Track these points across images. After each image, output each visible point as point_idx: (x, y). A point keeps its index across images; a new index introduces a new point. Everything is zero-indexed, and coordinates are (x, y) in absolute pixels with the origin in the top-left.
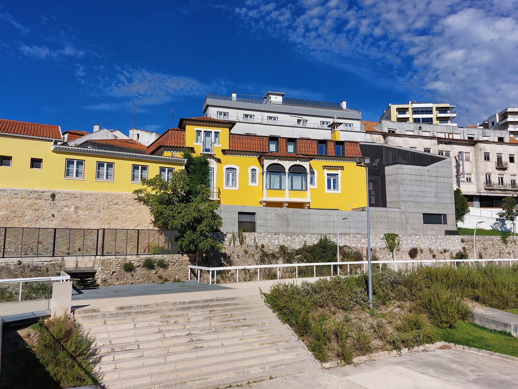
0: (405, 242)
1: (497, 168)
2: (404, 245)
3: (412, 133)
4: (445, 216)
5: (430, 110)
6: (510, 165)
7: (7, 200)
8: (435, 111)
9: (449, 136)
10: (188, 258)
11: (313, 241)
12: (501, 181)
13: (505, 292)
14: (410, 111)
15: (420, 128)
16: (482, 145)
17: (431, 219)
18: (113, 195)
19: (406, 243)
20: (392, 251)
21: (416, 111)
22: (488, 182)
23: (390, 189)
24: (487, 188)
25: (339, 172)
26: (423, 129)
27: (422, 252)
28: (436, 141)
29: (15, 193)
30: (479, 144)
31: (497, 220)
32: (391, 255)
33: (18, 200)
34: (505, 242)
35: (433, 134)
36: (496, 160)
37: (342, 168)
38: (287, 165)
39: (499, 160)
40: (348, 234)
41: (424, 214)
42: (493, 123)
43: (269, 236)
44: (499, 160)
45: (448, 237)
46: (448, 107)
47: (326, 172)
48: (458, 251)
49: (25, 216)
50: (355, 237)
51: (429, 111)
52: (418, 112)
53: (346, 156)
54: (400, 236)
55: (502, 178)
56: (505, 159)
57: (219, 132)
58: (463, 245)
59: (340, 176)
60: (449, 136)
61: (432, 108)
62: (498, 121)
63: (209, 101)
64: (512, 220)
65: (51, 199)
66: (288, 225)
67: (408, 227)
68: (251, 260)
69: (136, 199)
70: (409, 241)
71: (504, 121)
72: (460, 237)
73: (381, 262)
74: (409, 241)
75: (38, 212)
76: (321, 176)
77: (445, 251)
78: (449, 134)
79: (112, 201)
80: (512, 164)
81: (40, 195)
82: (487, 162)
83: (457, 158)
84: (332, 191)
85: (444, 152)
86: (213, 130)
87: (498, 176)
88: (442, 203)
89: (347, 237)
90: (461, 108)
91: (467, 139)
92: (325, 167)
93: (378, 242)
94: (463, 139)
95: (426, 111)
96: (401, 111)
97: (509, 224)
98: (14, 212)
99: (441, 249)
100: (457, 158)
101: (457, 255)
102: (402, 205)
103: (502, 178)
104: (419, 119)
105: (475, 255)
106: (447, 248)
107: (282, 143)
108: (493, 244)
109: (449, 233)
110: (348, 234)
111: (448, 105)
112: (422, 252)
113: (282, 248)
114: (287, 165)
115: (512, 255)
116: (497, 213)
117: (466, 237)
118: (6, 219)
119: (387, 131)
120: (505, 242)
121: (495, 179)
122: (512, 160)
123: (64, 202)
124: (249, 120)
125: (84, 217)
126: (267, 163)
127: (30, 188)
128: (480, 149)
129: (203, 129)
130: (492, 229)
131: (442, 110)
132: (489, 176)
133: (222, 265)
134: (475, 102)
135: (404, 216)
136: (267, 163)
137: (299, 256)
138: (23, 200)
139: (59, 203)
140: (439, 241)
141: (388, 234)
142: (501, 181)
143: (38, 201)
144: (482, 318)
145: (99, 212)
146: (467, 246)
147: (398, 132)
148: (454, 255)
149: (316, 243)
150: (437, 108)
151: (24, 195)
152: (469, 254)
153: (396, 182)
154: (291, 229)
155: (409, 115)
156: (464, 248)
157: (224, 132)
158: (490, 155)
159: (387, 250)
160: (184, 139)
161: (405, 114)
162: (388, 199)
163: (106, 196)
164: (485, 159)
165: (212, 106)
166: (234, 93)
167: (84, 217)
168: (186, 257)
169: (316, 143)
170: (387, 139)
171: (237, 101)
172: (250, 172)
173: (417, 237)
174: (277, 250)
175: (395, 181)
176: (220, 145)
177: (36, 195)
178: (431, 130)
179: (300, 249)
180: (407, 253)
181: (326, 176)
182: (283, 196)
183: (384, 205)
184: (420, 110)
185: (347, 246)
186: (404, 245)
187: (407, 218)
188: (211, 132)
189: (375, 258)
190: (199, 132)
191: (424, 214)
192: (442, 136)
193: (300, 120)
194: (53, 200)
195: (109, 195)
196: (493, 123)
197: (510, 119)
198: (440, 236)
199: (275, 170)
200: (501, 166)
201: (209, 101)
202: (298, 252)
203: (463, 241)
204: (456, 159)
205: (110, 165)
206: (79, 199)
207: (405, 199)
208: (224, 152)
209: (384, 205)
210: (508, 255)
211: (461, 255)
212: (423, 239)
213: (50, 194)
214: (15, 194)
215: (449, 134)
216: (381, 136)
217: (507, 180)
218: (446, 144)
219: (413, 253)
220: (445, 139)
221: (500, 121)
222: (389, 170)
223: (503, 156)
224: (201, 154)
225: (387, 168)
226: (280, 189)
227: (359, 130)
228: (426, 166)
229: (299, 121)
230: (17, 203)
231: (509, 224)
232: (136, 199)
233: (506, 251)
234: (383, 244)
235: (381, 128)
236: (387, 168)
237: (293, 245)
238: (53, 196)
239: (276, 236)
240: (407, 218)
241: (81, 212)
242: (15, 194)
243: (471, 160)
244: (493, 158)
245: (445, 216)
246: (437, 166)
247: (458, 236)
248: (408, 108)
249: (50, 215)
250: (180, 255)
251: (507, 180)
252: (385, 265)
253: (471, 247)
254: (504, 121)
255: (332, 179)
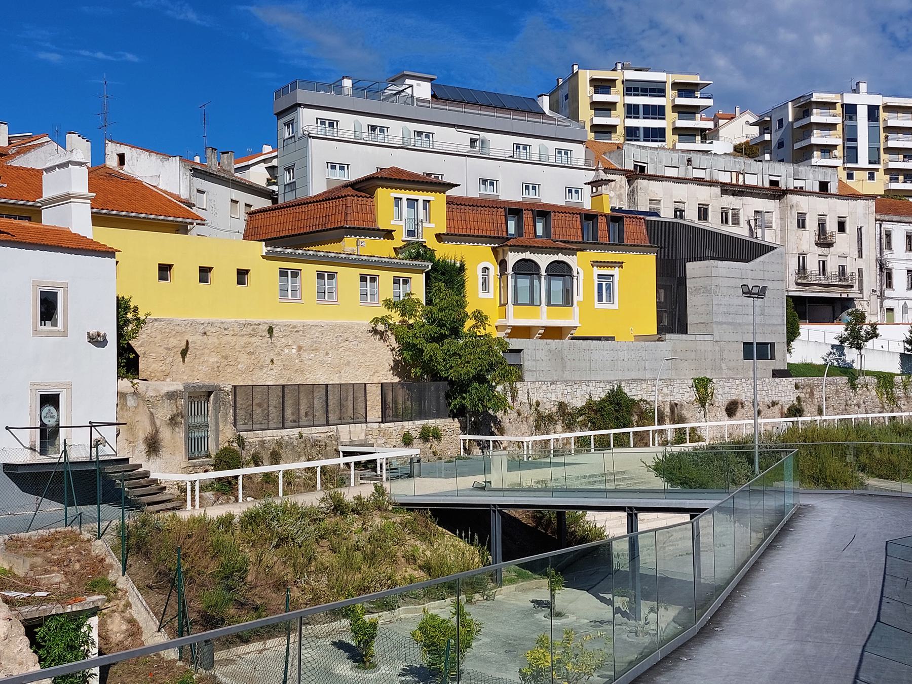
0: (721, 391)
1: (817, 244)
2: (719, 397)
3: (672, 173)
4: (773, 345)
5: (660, 86)
6: (839, 238)
7: (216, 340)
8: (670, 92)
9: (737, 179)
10: (459, 425)
11: (599, 393)
12: (823, 266)
13: (894, 458)
14: (619, 86)
15: (689, 161)
16: (793, 199)
17: (758, 351)
18: (342, 326)
19: (722, 394)
20: (703, 406)
21: (631, 88)
22: (802, 269)
23: (694, 301)
24: (799, 281)
25: (615, 271)
26: (695, 163)
27: (742, 407)
28: (717, 190)
29: (225, 328)
30: (789, 196)
31: (833, 346)
32: (702, 412)
33: (229, 338)
34: (854, 387)
35: (711, 173)
36: (817, 228)
37: (620, 264)
38: (543, 260)
39: (822, 226)
40: (645, 380)
41: (744, 343)
42: (781, 122)
43: (544, 387)
44: (822, 226)
45: (777, 380)
46: (698, 84)
47: (597, 271)
48: (791, 403)
49: (239, 363)
50: (654, 385)
51: (658, 90)
52: (636, 89)
53: (625, 242)
54: (714, 381)
55: (824, 262)
56: (831, 226)
57: (429, 201)
58: (798, 393)
59: (616, 278)
60: (737, 179)
61: (665, 82)
62: (790, 120)
63: (302, 95)
64: (859, 348)
65: (268, 336)
66: (564, 368)
67: (723, 366)
68: (524, 427)
69: (370, 331)
70: (727, 389)
71: (804, 122)
72: (792, 380)
73: (687, 426)
74: (727, 389)
75: (253, 357)
76: (588, 277)
77: (774, 404)
78: (738, 173)
79: (343, 333)
80: (842, 235)
81: (250, 329)
82: (801, 231)
83: (752, 223)
84: (605, 305)
85: (730, 212)
86: (421, 196)
87: (818, 258)
88: (769, 325)
89: (644, 386)
90: (665, 32)
91: (767, 185)
92: (596, 264)
93: (685, 394)
94: (760, 185)
95: (653, 90)
96: (602, 86)
97: (851, 355)
98: (226, 358)
99: (768, 400)
100: (752, 223)
101: (789, 409)
102: (717, 330)
103: (824, 262)
104: (636, 107)
105: (814, 409)
106: (776, 399)
107: (527, 217)
108: (837, 391)
109: (777, 374)
110: (645, 380)
111: (696, 79)
112: (742, 407)
113: (562, 406)
114: (543, 260)
115: (862, 409)
116: (836, 335)
117: (801, 380)
118: (216, 369)
119: (632, 168)
120: (854, 387)
121: (812, 266)
122: (842, 227)
123: (283, 340)
124: (380, 138)
125: (310, 363)
126: (513, 258)
127: (242, 320)
128: (792, 207)
129: (405, 195)
130: (824, 362)
131: (685, 89)
132: (804, 258)
133: (492, 434)
134: (699, 18)
135: (717, 348)
136: (513, 258)
137: (581, 418)
138: (234, 338)
139: (280, 340)
140: (765, 388)
141: (698, 379)
142: (823, 266)
143: (253, 339)
144: (877, 488)
145: (327, 354)
146: (802, 395)
147: (650, 171)
148: (785, 410)
149: (603, 396)
150: (675, 85)
151: (237, 330)
152: (805, 408)
153: (707, 290)
154: (567, 375)
155: (615, 96)
156: (798, 398)
157: (438, 200)
158: (807, 216)
159: (697, 405)
160: (373, 213)
161: (609, 93)
162: (690, 319)
163: (333, 327)
164: (799, 227)
165: (307, 106)
166: (348, 78)
167: (310, 363)
168: (456, 424)
169: (579, 219)
170: (635, 184)
171: (353, 95)
172: (480, 273)
173: (737, 382)
174: (554, 410)
175: (706, 287)
176: (432, 225)
177: (249, 330)
178: (708, 166)
179: (583, 407)
180: (724, 408)
181: (596, 277)
182: (537, 316)
183: (685, 331)
184: (640, 86)
185: (645, 401)
186: (719, 397)
187: (721, 351)
188: (417, 200)
189: (682, 420)
190: (398, 200)
191: (744, 343)
192: (725, 178)
193: (476, 140)
194: (271, 337)
195: (337, 326)
196: (781, 122)
197: (817, 117)
198: (767, 380)
199: (526, 269)
200: (824, 241)
201: (302, 95)
202: (581, 412)
203: (797, 387)
204: (750, 226)
205: (332, 276)
206: (301, 333)
207: (720, 319)
208: (439, 237)
209: (685, 331)
210: (856, 408)
211: (795, 411)
212: (744, 385)
213: (266, 327)
214: (225, 329)
215: (738, 173)
216: (624, 178)
217: (832, 268)
218: (733, 195)
219: (732, 409)
220: (731, 185)
221: (796, 119)
222: (692, 268)
223: (827, 219)
224: (403, 241)
225: (690, 266)
226: (532, 303)
227: (581, 163)
228: (747, 261)
229: (473, 141)
230: (228, 343)
231: (851, 355)
232: (370, 331)
233: (855, 402)
234: (691, 395)
235: (623, 164)
236: (690, 266)
237: (574, 401)
238: (270, 330)
239: (553, 387)
240: (721, 351)
241: (305, 355)
242: (225, 329)
243: (774, 227)
244: (812, 224)
245: (773, 345)
246: (763, 262)
247: (791, 379)
248: (615, 80)
249: (268, 362)
250: (450, 420)
251: (832, 268)
252: (693, 429)
253: (807, 396)
254: (804, 122)
255: (604, 284)
